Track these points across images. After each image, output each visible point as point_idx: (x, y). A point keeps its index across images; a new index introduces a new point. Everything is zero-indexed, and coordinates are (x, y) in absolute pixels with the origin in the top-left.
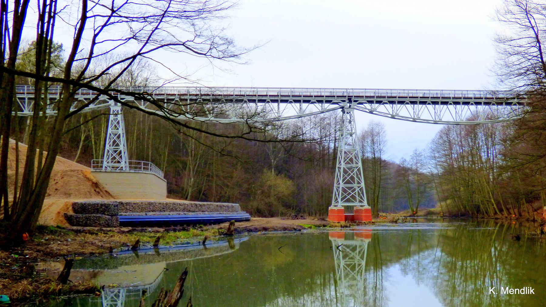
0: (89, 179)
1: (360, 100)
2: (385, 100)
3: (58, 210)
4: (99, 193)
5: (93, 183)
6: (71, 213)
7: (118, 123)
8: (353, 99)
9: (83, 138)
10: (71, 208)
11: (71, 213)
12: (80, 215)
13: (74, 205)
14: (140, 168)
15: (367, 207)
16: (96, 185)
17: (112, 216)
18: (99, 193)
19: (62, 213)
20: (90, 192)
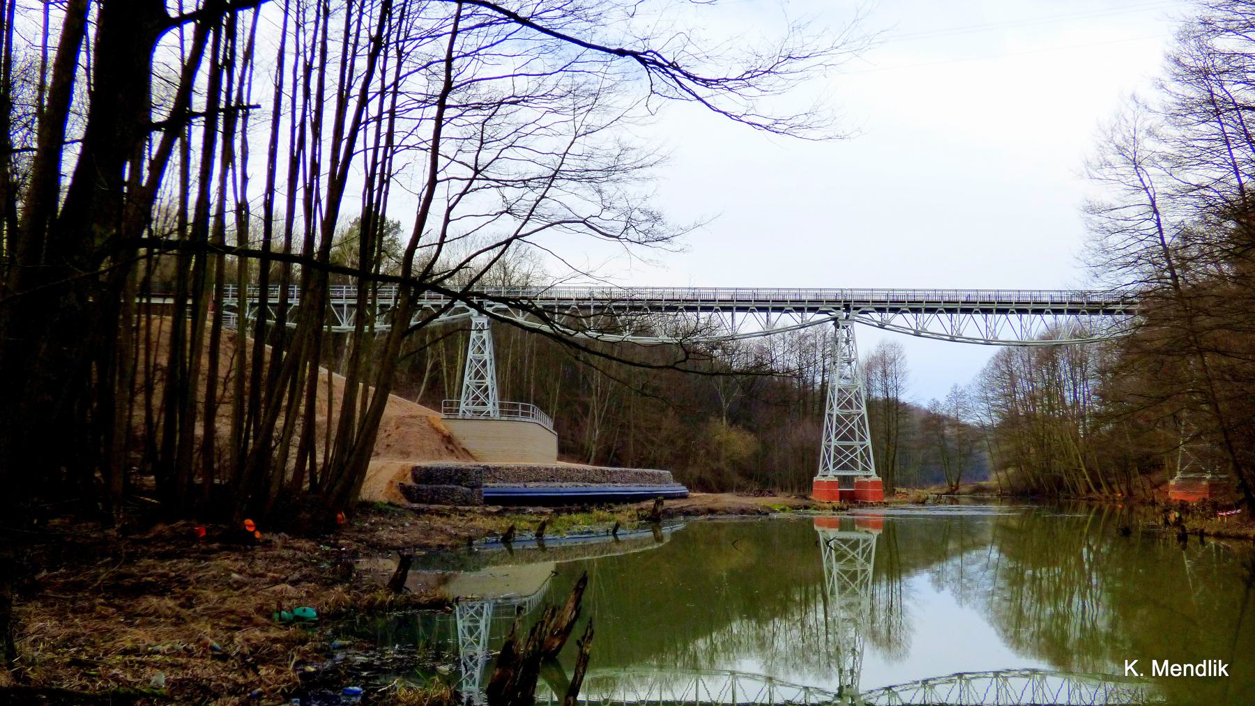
0: (437, 430)
1: (864, 307)
2: (904, 307)
3: (390, 478)
4: (452, 451)
5: (444, 436)
6: (409, 482)
7: (484, 343)
8: (852, 305)
9: (429, 367)
10: (409, 475)
11: (409, 482)
12: (424, 487)
13: (415, 469)
14: (517, 413)
15: (875, 477)
16: (448, 440)
17: (472, 488)
18: (452, 451)
19: (397, 482)
20: (439, 451)
